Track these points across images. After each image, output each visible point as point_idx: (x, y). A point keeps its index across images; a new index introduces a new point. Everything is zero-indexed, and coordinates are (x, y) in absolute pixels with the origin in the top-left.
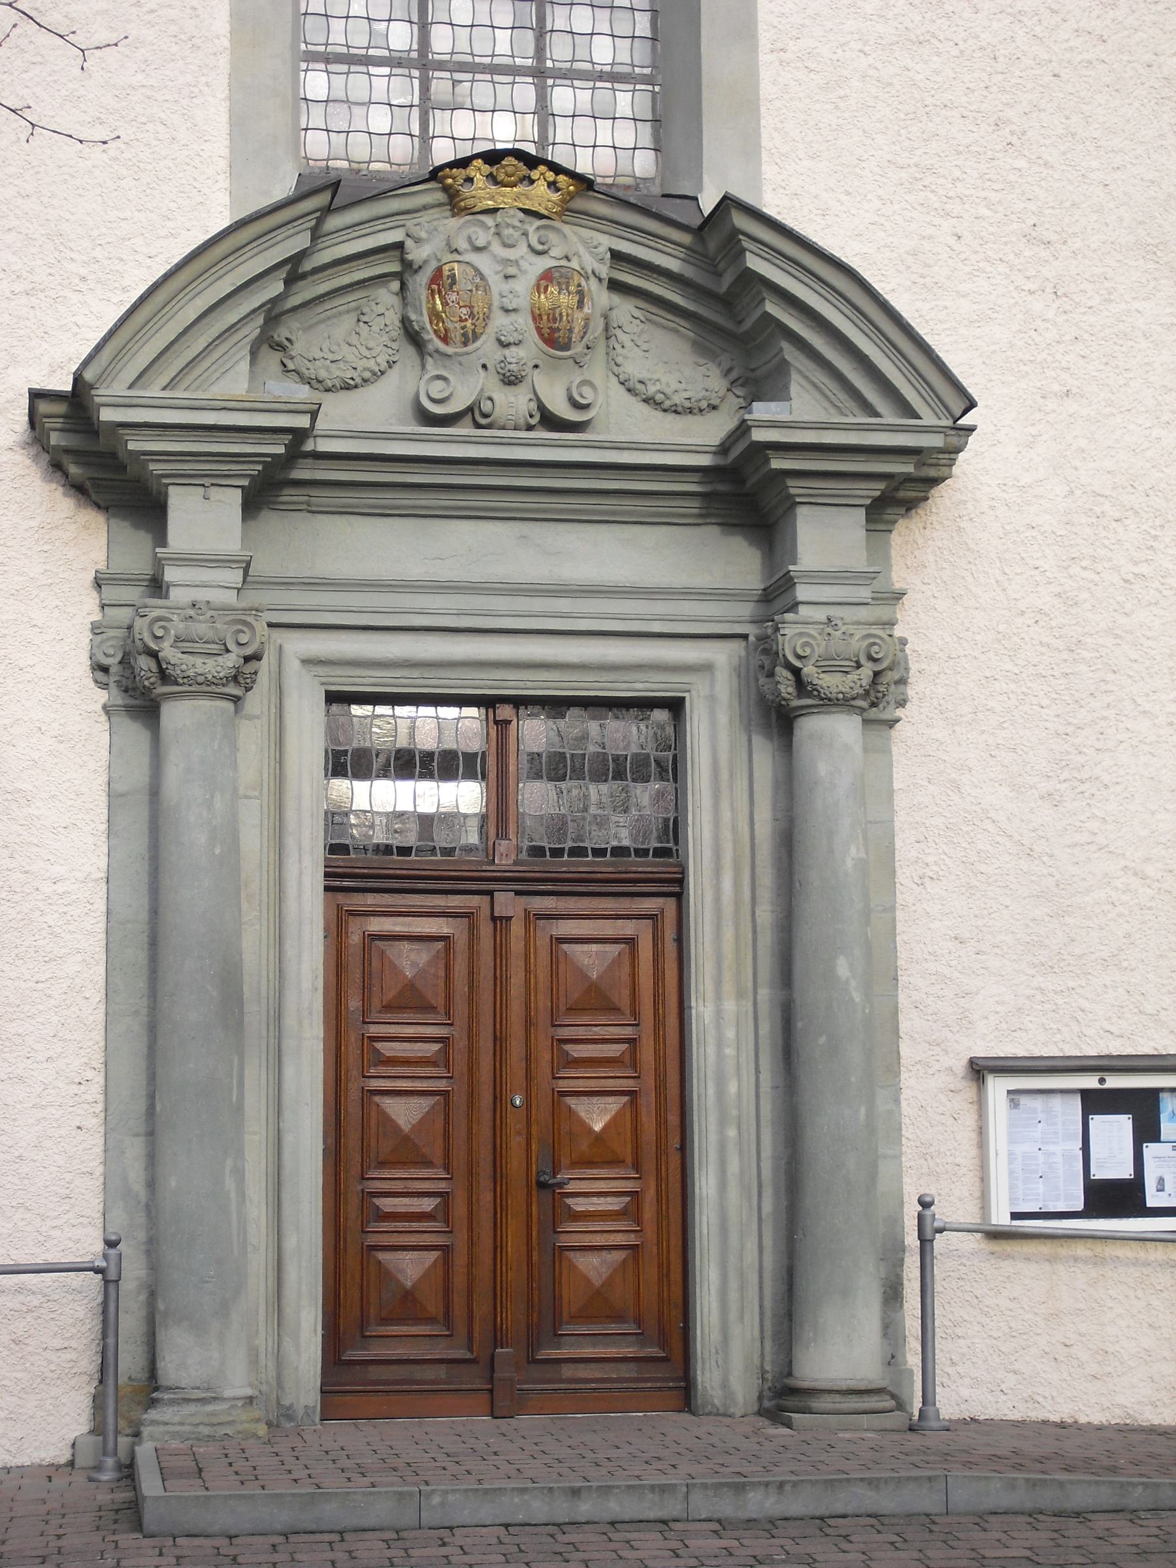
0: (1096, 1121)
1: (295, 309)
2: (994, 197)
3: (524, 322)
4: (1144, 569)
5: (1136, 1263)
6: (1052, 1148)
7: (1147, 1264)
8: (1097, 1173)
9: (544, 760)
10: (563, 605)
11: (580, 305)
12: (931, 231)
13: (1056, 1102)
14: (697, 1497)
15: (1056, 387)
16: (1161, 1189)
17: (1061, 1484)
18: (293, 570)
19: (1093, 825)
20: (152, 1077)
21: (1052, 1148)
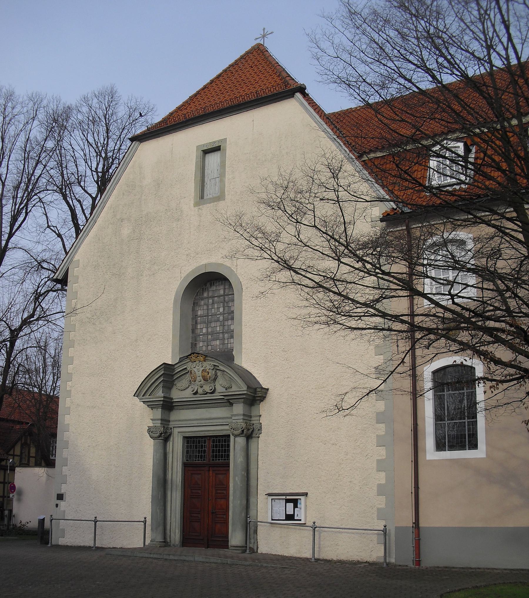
0: (287, 504)
1: (175, 379)
2: (278, 344)
3: (201, 377)
4: (300, 407)
5: (294, 529)
6: (280, 509)
7: (296, 529)
8: (287, 513)
9: (467, 446)
10: (211, 421)
11: (208, 374)
12: (268, 352)
13: (281, 501)
14: (164, 556)
15: (286, 376)
16: (297, 516)
17: (209, 558)
18: (177, 419)
19: (290, 453)
20: (248, 500)
21: (280, 509)
